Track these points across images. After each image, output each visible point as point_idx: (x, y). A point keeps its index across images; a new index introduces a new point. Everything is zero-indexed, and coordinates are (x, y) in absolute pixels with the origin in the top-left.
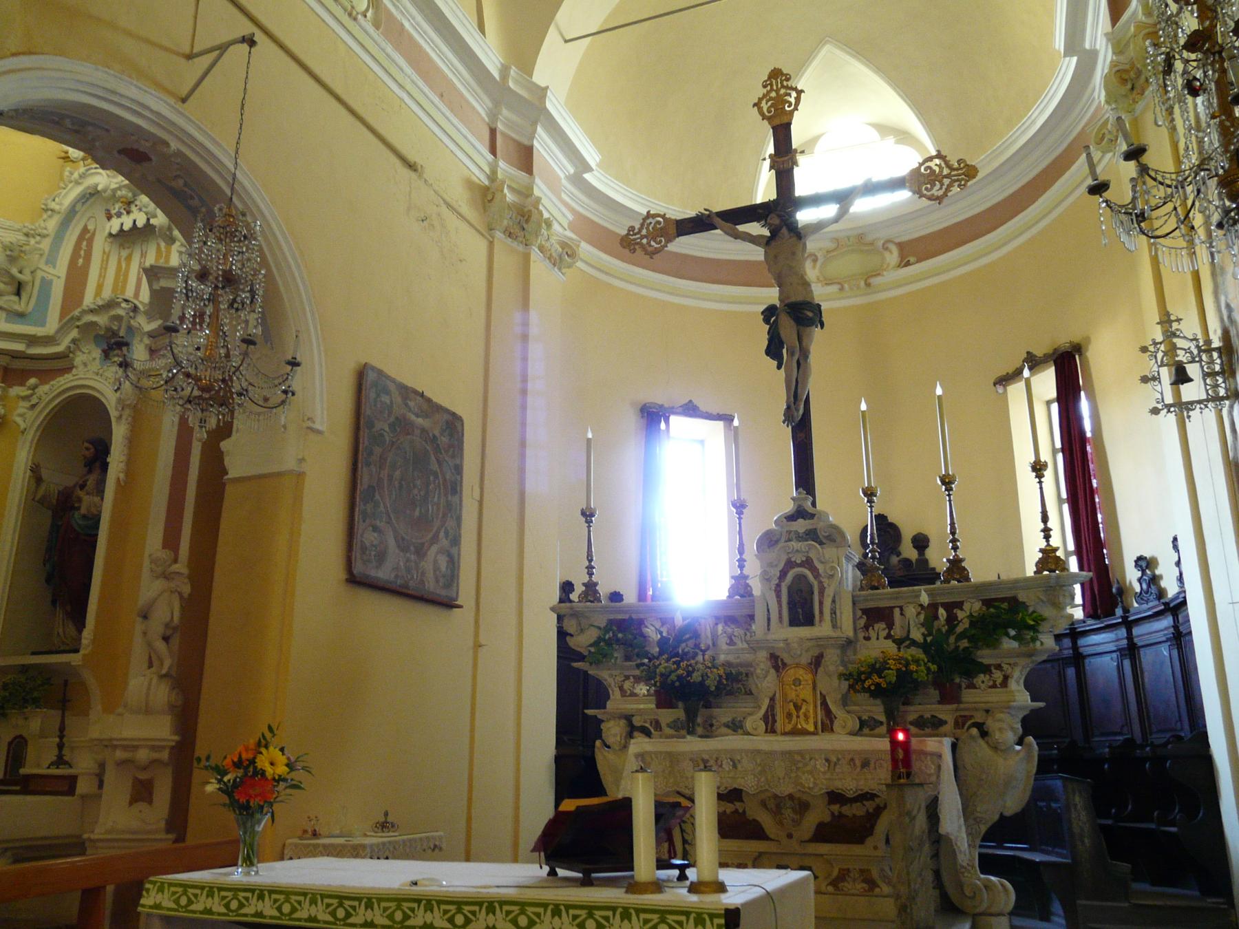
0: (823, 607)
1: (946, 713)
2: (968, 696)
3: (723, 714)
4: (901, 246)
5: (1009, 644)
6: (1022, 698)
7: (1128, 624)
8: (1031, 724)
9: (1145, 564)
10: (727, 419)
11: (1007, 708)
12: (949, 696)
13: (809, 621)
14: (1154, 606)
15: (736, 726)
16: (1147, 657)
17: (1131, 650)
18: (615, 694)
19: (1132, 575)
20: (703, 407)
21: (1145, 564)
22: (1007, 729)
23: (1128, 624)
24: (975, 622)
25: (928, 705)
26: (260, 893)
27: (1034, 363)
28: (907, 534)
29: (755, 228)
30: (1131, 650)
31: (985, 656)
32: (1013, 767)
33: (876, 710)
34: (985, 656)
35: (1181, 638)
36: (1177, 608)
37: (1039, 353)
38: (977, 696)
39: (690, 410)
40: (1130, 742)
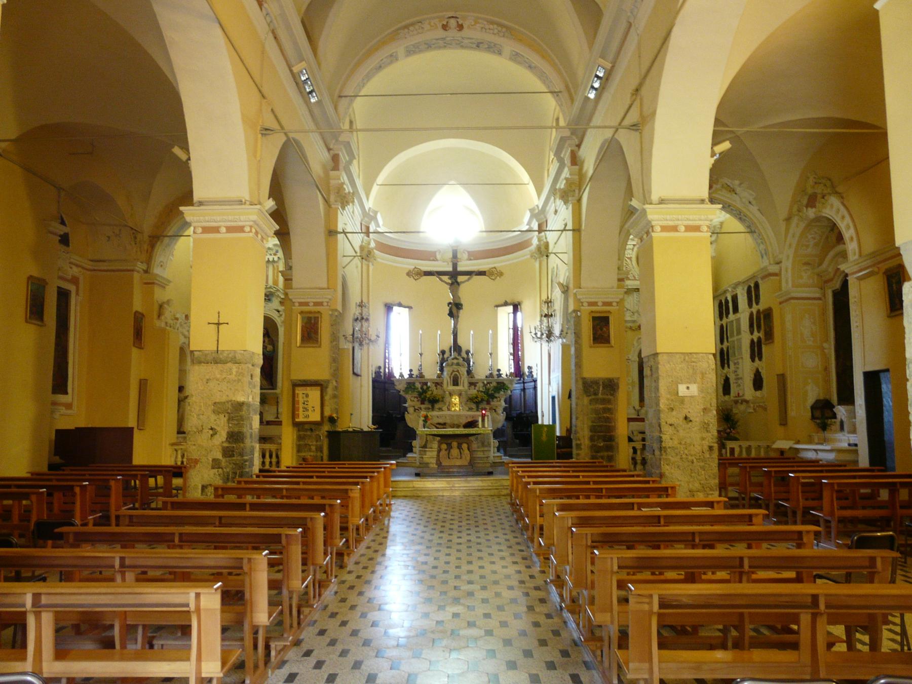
0: (461, 381)
1: (488, 407)
2: (492, 403)
3: (437, 406)
4: (469, 252)
5: (502, 393)
6: (503, 404)
7: (524, 383)
8: (505, 409)
9: (530, 368)
10: (410, 308)
11: (500, 405)
12: (488, 403)
13: (457, 385)
14: (530, 379)
15: (440, 409)
16: (527, 391)
17: (524, 389)
18: (409, 401)
19: (526, 370)
20: (403, 303)
21: (530, 368)
22: (500, 410)
23: (524, 383)
24: (495, 387)
25: (484, 405)
26: (576, 387)
27: (506, 304)
28: (464, 349)
29: (446, 278)
30: (524, 389)
31: (497, 395)
32: (501, 417)
33: (474, 406)
34: (497, 395)
35: (535, 388)
36: (535, 381)
37: (509, 301)
38: (494, 403)
39: (400, 305)
40: (521, 413)
